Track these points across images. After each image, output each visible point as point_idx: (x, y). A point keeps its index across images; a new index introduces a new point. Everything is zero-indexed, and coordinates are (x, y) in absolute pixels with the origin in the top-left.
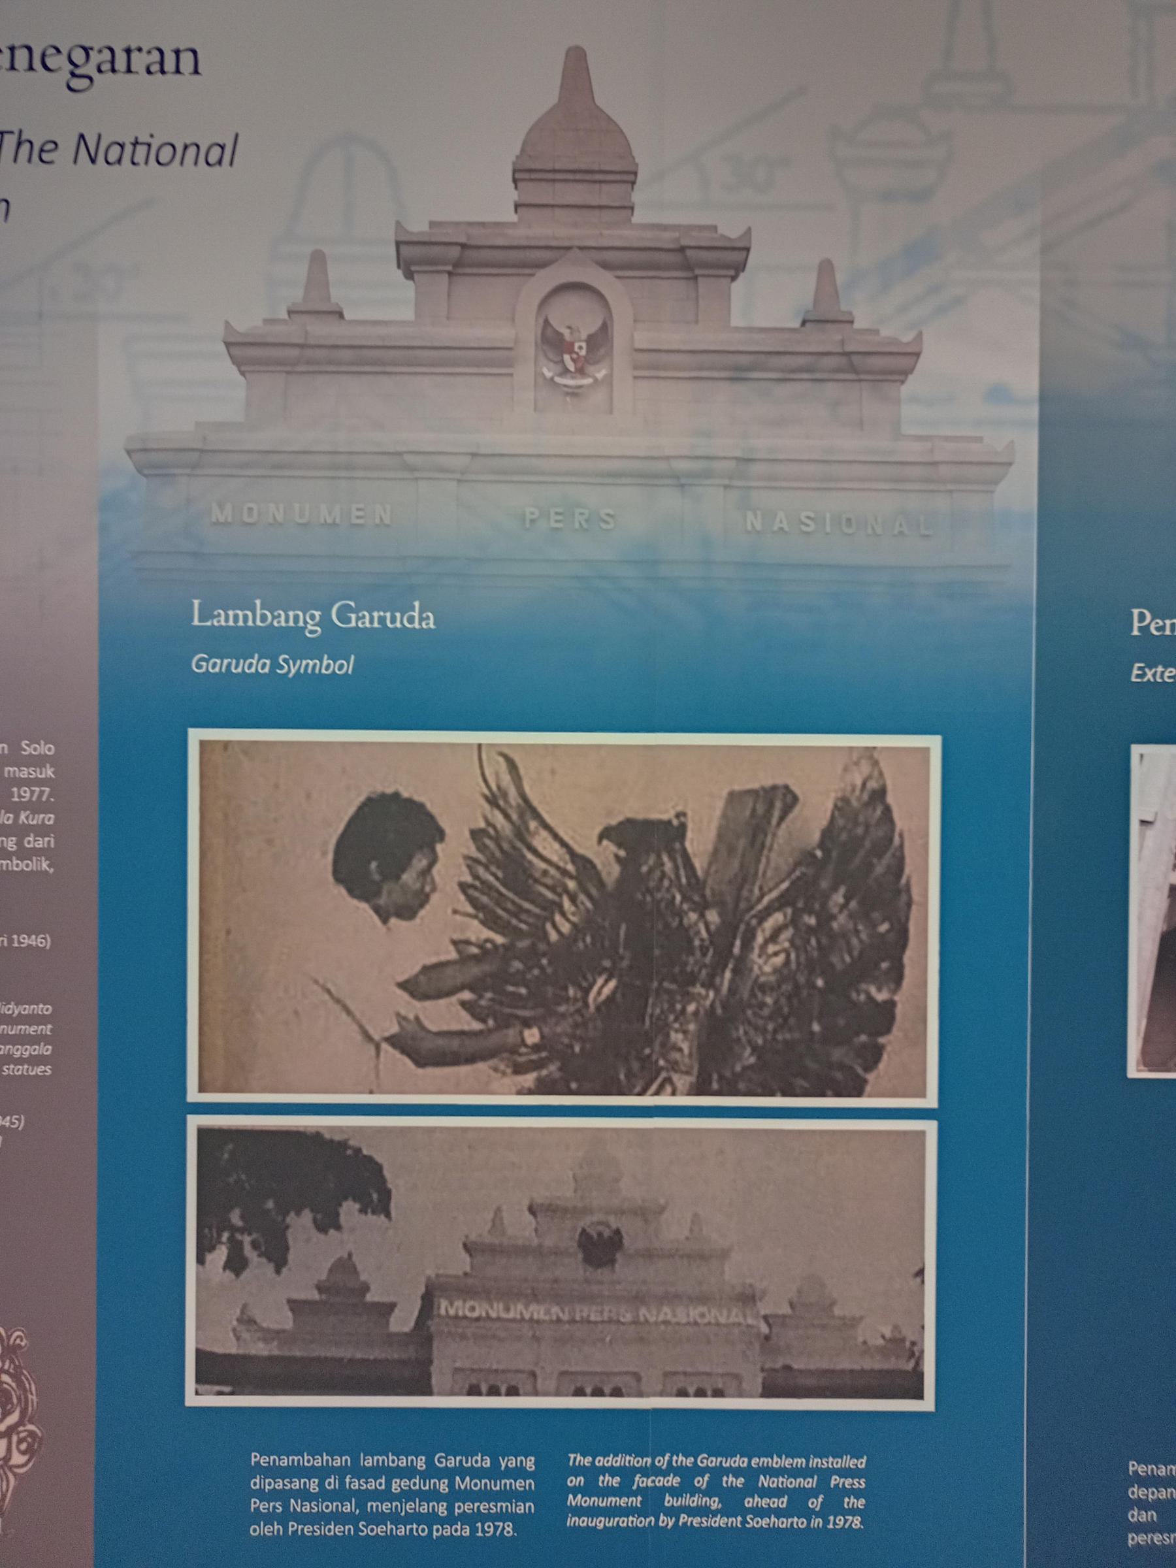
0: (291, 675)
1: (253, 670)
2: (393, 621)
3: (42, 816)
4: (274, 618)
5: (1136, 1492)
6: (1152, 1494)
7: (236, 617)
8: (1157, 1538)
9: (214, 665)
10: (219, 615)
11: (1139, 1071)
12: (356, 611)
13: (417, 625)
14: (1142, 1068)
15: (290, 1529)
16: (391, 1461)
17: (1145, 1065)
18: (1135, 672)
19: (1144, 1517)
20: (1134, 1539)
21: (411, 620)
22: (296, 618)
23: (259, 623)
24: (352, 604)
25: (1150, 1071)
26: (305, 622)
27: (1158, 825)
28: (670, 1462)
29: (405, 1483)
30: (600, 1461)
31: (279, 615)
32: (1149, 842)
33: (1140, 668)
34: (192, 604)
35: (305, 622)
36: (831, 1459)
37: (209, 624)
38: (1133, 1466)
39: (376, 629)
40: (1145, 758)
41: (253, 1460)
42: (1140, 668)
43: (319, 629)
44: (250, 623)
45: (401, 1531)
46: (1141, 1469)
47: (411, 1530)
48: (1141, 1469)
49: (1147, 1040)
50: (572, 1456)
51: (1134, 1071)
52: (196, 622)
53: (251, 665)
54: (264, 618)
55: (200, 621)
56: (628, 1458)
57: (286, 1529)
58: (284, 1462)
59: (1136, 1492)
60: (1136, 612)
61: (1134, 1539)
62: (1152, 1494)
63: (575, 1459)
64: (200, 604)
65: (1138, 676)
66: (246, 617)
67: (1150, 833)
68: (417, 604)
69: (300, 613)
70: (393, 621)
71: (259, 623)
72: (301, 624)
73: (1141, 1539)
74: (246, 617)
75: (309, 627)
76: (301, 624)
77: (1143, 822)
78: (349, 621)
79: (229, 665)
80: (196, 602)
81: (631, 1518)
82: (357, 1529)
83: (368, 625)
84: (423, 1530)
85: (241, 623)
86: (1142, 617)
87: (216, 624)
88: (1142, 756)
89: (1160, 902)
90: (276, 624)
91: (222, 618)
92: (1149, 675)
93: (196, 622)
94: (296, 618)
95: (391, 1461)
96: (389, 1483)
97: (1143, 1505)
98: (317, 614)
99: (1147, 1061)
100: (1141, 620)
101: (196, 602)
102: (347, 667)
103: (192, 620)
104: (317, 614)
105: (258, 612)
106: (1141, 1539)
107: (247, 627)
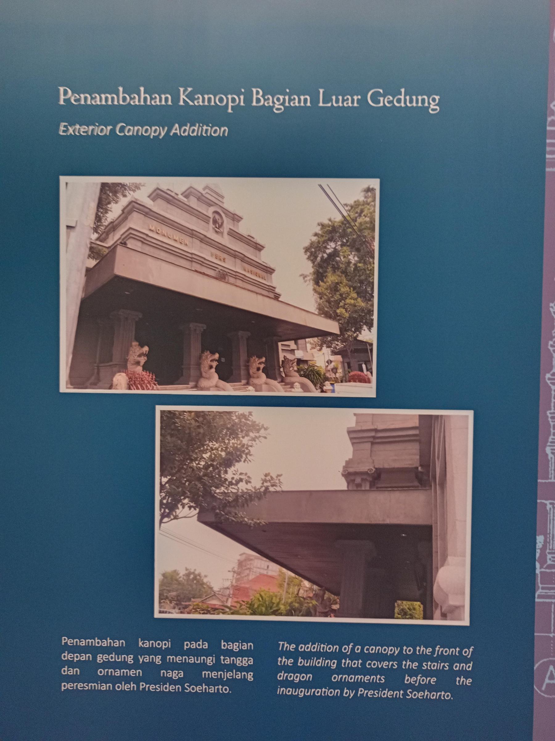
0: (161, 137)
1: (186, 134)
2: (86, 98)
3: (313, 690)
4: (131, 99)
5: (66, 656)
6: (76, 657)
7: (107, 99)
8: (80, 686)
9: (433, 695)
10: (199, 98)
11: (67, 388)
12: (384, 96)
13: (341, 105)
14: (69, 386)
15: (141, 687)
16: (96, 642)
17: (71, 384)
18: (62, 128)
19: (71, 672)
20: (66, 686)
21: (233, 100)
22: (423, 101)
23: (121, 103)
24: (381, 91)
25: (74, 388)
26: (429, 103)
27: (78, 228)
28: (353, 649)
29: (105, 657)
30: (302, 648)
31: (96, 97)
32: (72, 240)
33: (65, 126)
34: (319, 92)
35: (429, 103)
36: (429, 663)
37: (329, 105)
38: (65, 640)
39: (355, 107)
40: (68, 185)
41: (63, 641)
42: (65, 126)
43: (437, 107)
44: (116, 103)
45: (212, 690)
46: (70, 642)
47: (218, 689)
48: (70, 642)
49: (73, 368)
50: (281, 643)
51: (64, 388)
52: (321, 104)
53: (384, 694)
54: (124, 99)
55: (323, 103)
56: (322, 646)
57: (138, 687)
58: (83, 643)
59: (66, 656)
60: (62, 89)
61: (66, 686)
62: (76, 657)
63: (283, 645)
64: (323, 92)
65: (64, 131)
66: (113, 99)
67: (73, 234)
68: (403, 90)
69: (426, 97)
70: (86, 98)
71: (121, 103)
72: (426, 105)
73: (69, 686)
74: (113, 99)
75: (432, 107)
76: (426, 105)
77: (68, 227)
78: (379, 102)
79: (314, 692)
80: (321, 91)
81: (323, 690)
82: (184, 688)
83: (297, 104)
84: (226, 690)
85: (110, 103)
86: (66, 93)
87: (196, 104)
88: (67, 184)
89: (80, 279)
90: (266, 104)
91: (158, 100)
92: (71, 131)
93: (321, 104)
94: (423, 101)
95: (96, 642)
96: (363, 664)
97: (71, 664)
98: (437, 98)
99: (73, 381)
100: (65, 95)
101: (321, 91)
102: (224, 130)
103: (319, 103)
104: (437, 98)
105: (121, 95)
106: (69, 686)
107: (113, 105)
